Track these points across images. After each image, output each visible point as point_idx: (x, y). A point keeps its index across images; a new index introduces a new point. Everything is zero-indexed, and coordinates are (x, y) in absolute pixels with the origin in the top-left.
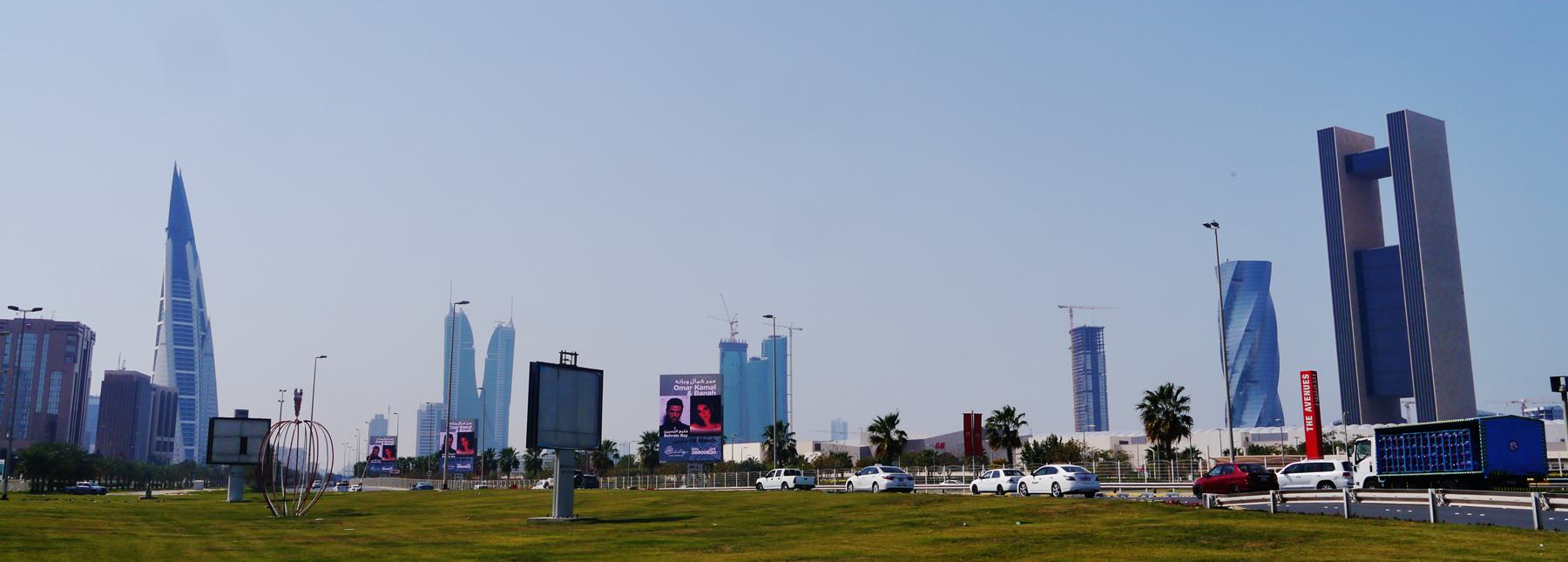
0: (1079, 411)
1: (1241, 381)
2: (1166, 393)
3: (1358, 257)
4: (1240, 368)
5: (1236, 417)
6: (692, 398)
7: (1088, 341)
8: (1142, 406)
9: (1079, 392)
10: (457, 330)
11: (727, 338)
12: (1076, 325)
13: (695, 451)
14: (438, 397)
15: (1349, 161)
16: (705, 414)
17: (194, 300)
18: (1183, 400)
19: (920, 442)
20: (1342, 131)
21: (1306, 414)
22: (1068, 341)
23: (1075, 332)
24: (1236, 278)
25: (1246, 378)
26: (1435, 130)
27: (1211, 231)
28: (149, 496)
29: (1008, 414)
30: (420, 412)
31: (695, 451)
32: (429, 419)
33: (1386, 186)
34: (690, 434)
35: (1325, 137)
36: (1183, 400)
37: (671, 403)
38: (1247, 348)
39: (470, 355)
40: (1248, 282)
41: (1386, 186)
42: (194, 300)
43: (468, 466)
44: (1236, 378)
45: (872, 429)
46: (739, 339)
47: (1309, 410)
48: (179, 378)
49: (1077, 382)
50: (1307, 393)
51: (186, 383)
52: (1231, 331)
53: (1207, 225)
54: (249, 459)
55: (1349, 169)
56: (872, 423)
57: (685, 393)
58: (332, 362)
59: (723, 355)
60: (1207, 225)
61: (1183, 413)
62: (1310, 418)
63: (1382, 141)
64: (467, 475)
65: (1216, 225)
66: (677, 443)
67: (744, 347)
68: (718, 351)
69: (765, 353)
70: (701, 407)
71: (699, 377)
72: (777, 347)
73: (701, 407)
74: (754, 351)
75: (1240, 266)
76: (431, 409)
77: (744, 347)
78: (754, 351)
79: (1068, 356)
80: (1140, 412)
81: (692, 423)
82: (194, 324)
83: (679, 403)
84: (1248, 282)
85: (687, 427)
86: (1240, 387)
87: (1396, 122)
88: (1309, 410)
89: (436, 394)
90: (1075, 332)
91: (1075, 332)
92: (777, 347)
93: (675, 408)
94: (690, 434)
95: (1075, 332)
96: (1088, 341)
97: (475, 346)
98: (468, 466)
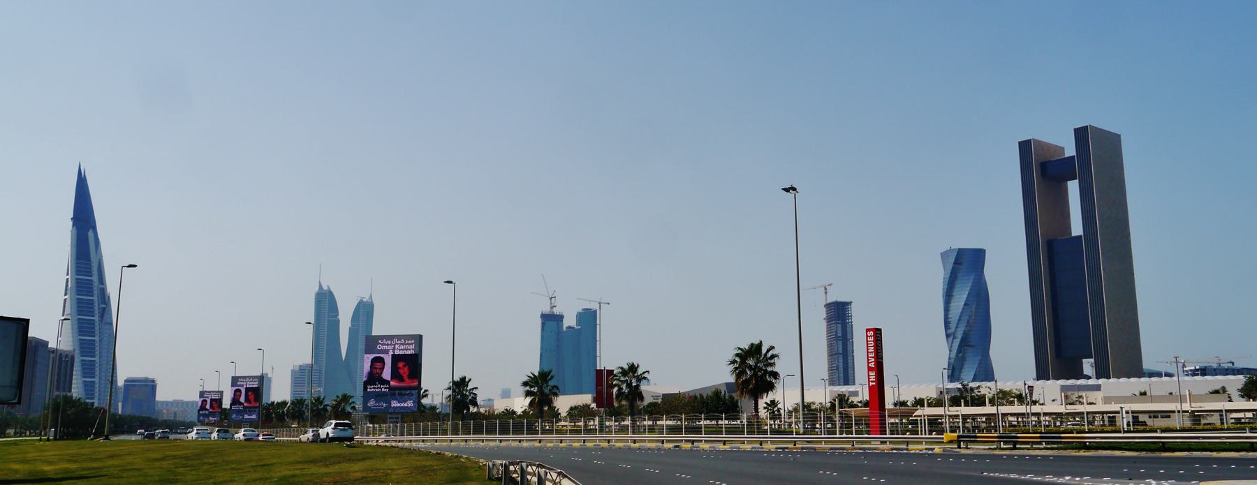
0: (831, 370)
1: (960, 346)
2: (755, 350)
3: (1050, 244)
4: (959, 335)
5: (956, 374)
6: (394, 356)
7: (839, 313)
8: (733, 362)
9: (832, 355)
10: (325, 303)
11: (547, 310)
12: (830, 301)
13: (395, 404)
14: (307, 359)
15: (1044, 167)
16: (404, 371)
17: (95, 278)
18: (773, 357)
19: (167, 403)
20: (1038, 143)
21: (870, 369)
22: (823, 313)
23: (829, 306)
24: (957, 262)
25: (965, 343)
26: (1112, 143)
27: (790, 195)
28: (316, 436)
29: (633, 368)
30: (293, 372)
31: (395, 404)
32: (300, 376)
33: (1073, 187)
34: (390, 388)
35: (1025, 147)
36: (773, 357)
37: (374, 361)
38: (965, 318)
39: (335, 324)
40: (967, 265)
41: (1073, 187)
42: (95, 278)
43: (254, 417)
44: (957, 343)
45: (525, 384)
46: (557, 311)
47: (872, 365)
48: (82, 343)
49: (830, 346)
50: (871, 349)
51: (86, 348)
52: (953, 305)
53: (787, 190)
54: (141, 415)
55: (1043, 173)
56: (526, 379)
57: (386, 352)
58: (191, 333)
59: (543, 324)
60: (787, 190)
61: (770, 369)
62: (873, 374)
63: (1070, 151)
64: (252, 424)
65: (794, 189)
66: (379, 396)
67: (561, 317)
68: (539, 321)
69: (579, 322)
70: (401, 365)
71: (399, 337)
72: (589, 318)
73: (401, 365)
74: (570, 321)
75: (961, 252)
76: (302, 369)
77: (561, 317)
78: (570, 321)
79: (824, 325)
80: (732, 367)
81: (392, 378)
82: (95, 298)
83: (381, 360)
84: (967, 265)
85: (388, 382)
86: (959, 351)
87: (1081, 134)
88: (872, 365)
89: (305, 357)
90: (829, 306)
91: (828, 306)
92: (589, 318)
93: (378, 365)
94: (390, 388)
95: (828, 306)
96: (839, 313)
97: (340, 317)
98: (254, 417)
